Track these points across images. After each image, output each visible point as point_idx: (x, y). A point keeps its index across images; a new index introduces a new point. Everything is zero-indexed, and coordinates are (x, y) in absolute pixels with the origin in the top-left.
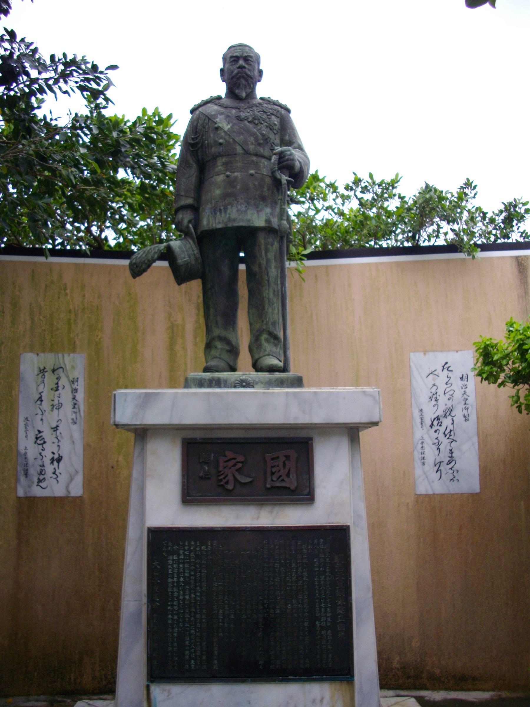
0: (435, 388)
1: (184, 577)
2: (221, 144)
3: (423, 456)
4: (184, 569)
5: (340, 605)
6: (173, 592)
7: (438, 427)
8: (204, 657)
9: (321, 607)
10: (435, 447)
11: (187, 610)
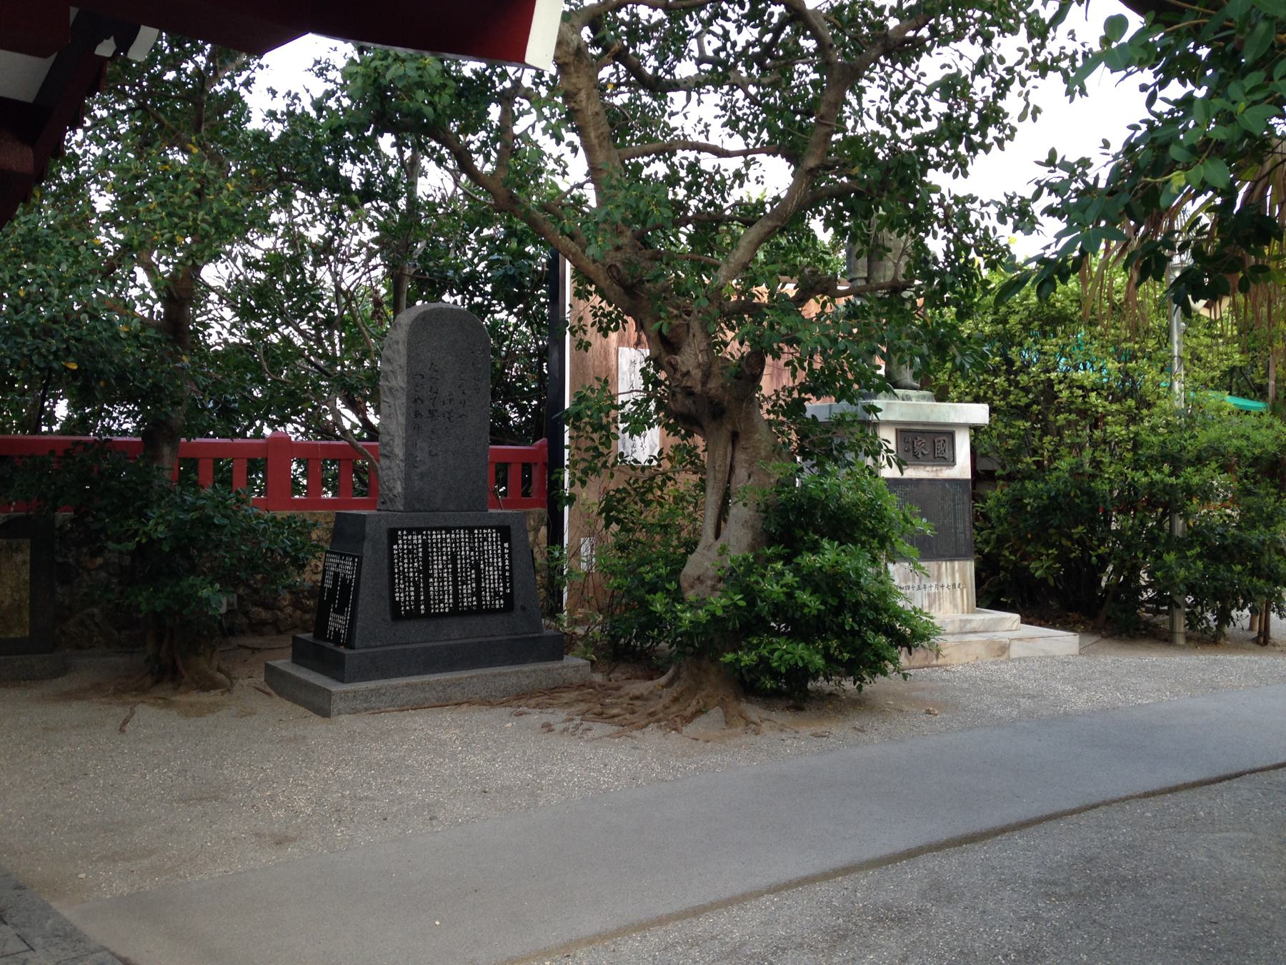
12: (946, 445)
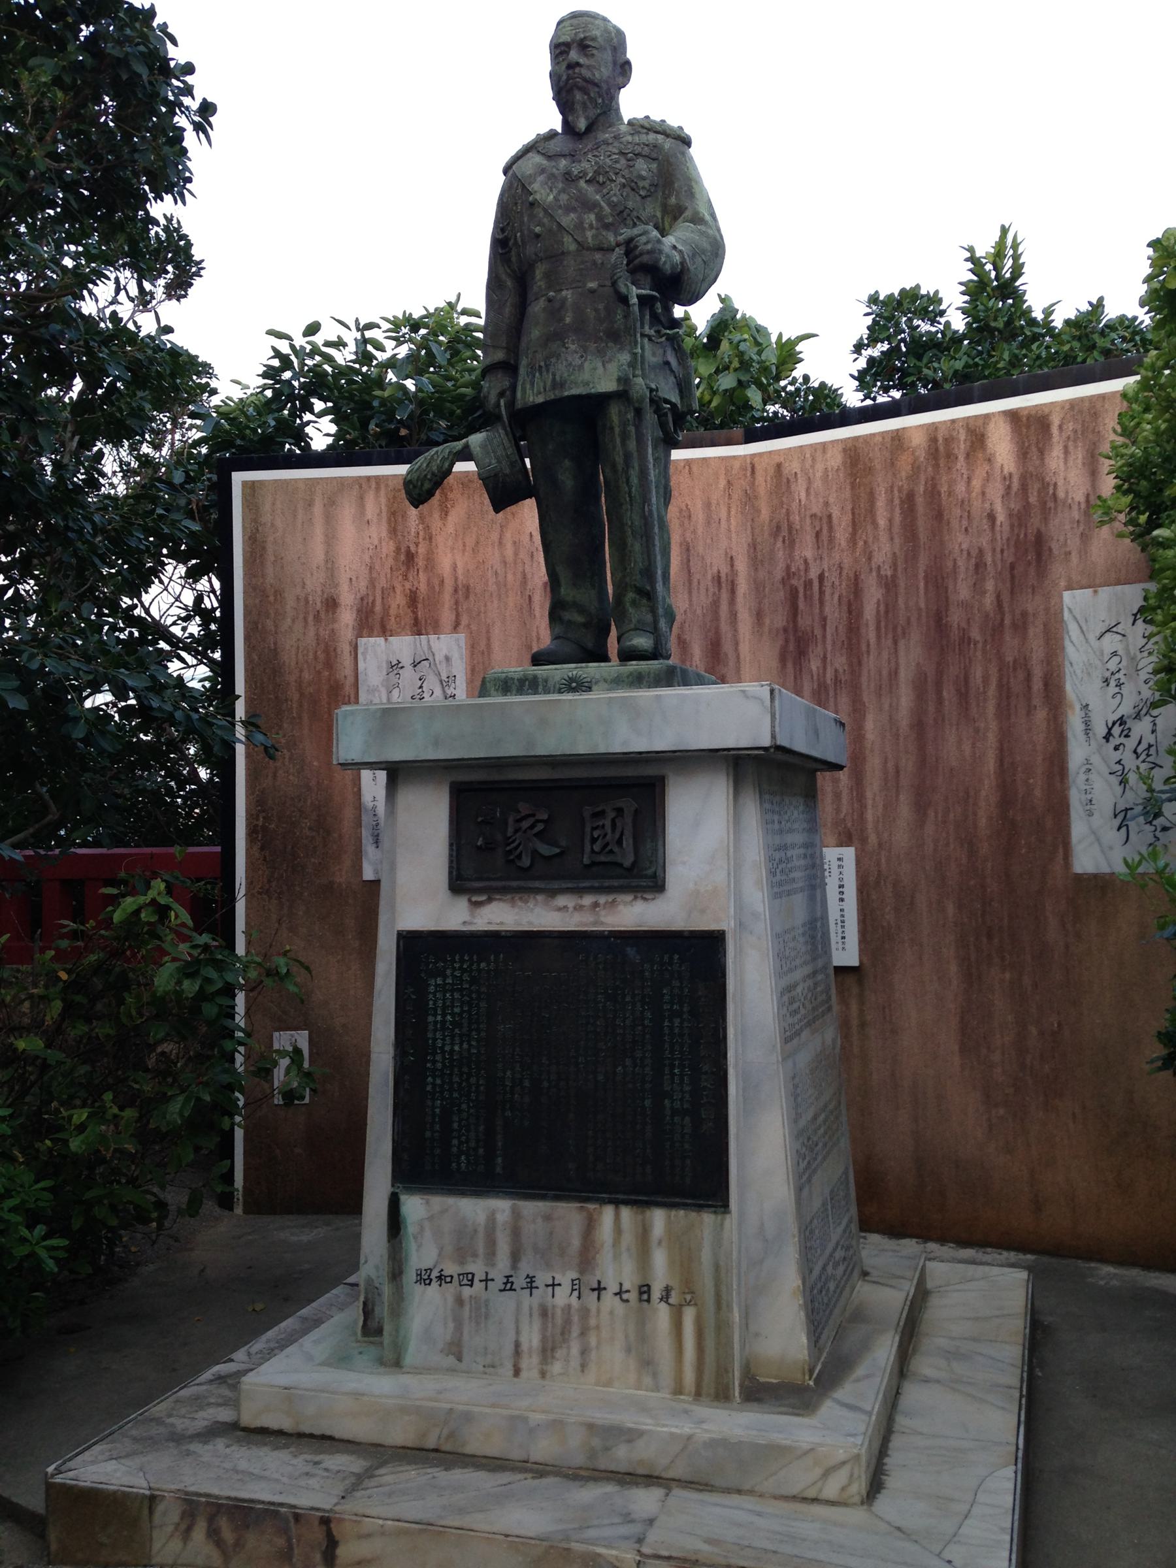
0: (1116, 659)
1: (453, 1014)
2: (538, 236)
3: (1089, 797)
4: (453, 999)
5: (706, 1073)
6: (435, 1040)
7: (1123, 740)
8: (481, 1151)
9: (673, 1075)
10: (1114, 780)
11: (456, 1070)
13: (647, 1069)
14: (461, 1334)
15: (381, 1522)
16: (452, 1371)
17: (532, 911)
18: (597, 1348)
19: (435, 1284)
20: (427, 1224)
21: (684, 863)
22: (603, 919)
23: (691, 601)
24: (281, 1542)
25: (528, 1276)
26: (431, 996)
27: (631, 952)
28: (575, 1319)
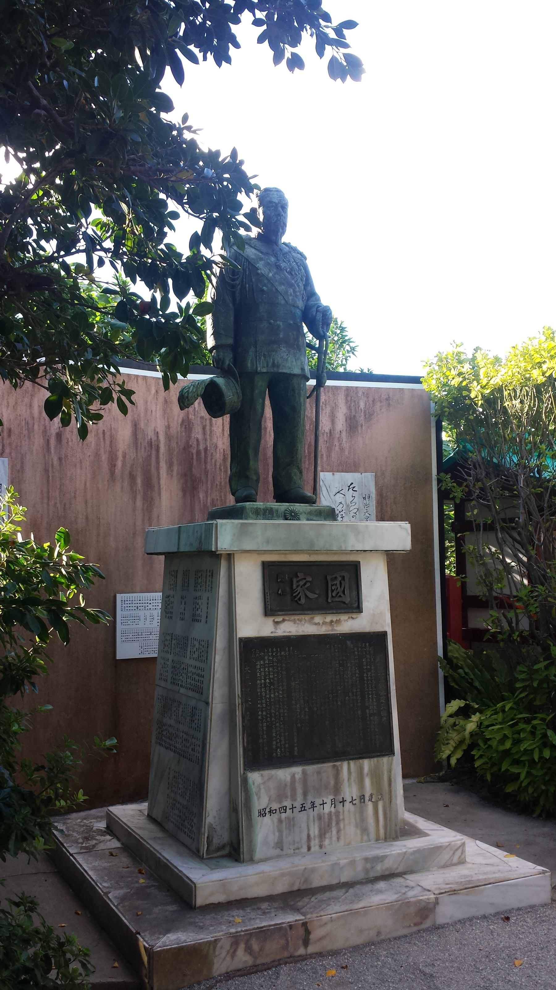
1: (269, 679)
6: (261, 692)
8: (287, 745)
12: (346, 583)
13: (358, 697)
14: (282, 837)
15: (330, 916)
16: (279, 856)
17: (304, 625)
18: (344, 828)
19: (268, 815)
20: (262, 787)
21: (368, 601)
22: (335, 628)
23: (137, 453)
24: (282, 942)
25: (312, 802)
26: (258, 670)
27: (349, 643)
28: (334, 818)
